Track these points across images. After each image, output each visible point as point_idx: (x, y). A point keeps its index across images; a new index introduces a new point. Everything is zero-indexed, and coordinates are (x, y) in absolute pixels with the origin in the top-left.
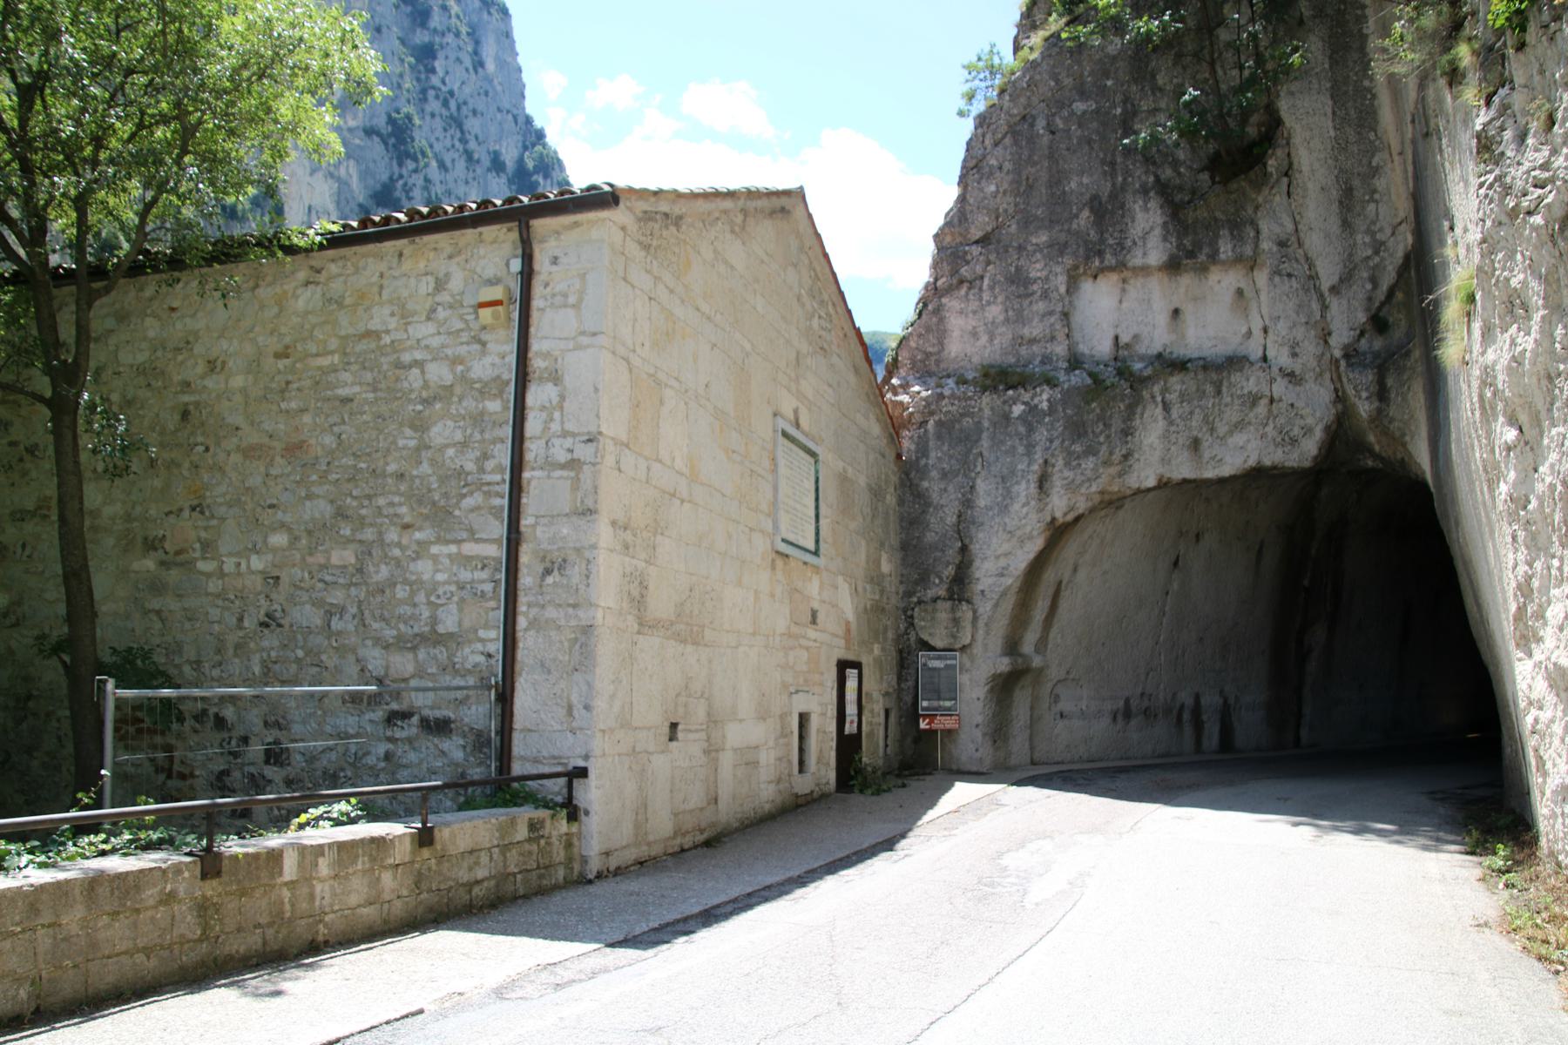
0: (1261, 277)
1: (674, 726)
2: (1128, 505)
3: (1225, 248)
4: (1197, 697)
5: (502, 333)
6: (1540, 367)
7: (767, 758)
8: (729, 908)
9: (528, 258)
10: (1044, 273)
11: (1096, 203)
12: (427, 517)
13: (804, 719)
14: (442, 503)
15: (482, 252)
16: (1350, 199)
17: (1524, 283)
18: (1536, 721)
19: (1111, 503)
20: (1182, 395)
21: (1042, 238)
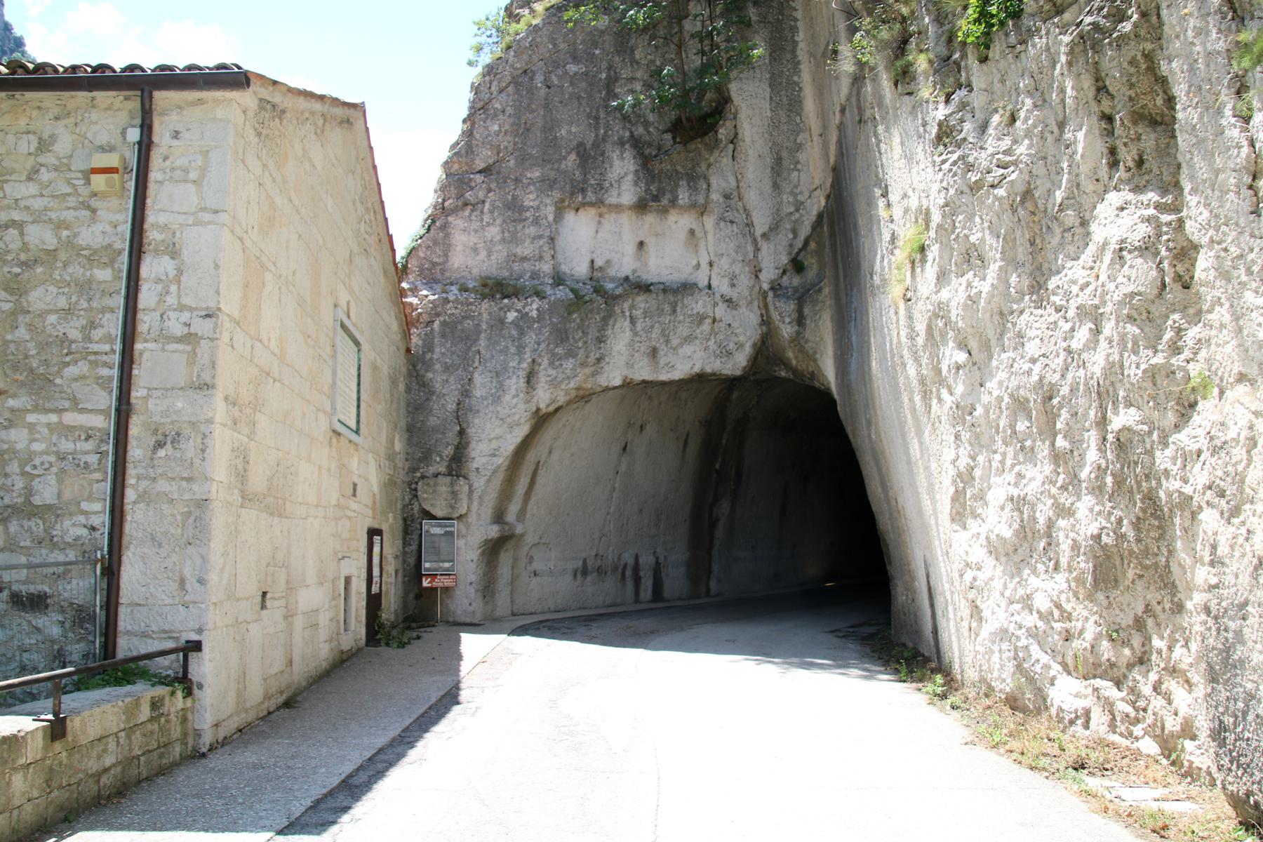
0: (709, 221)
1: (264, 594)
2: (594, 400)
3: (683, 196)
4: (637, 557)
5: (114, 202)
6: (993, 305)
7: (324, 619)
8: (363, 777)
9: (147, 128)
10: (536, 203)
11: (581, 149)
12: (23, 385)
13: (348, 580)
14: (41, 370)
15: (94, 117)
16: (780, 166)
17: (983, 240)
18: (975, 579)
19: (583, 397)
20: (645, 312)
21: (536, 174)
